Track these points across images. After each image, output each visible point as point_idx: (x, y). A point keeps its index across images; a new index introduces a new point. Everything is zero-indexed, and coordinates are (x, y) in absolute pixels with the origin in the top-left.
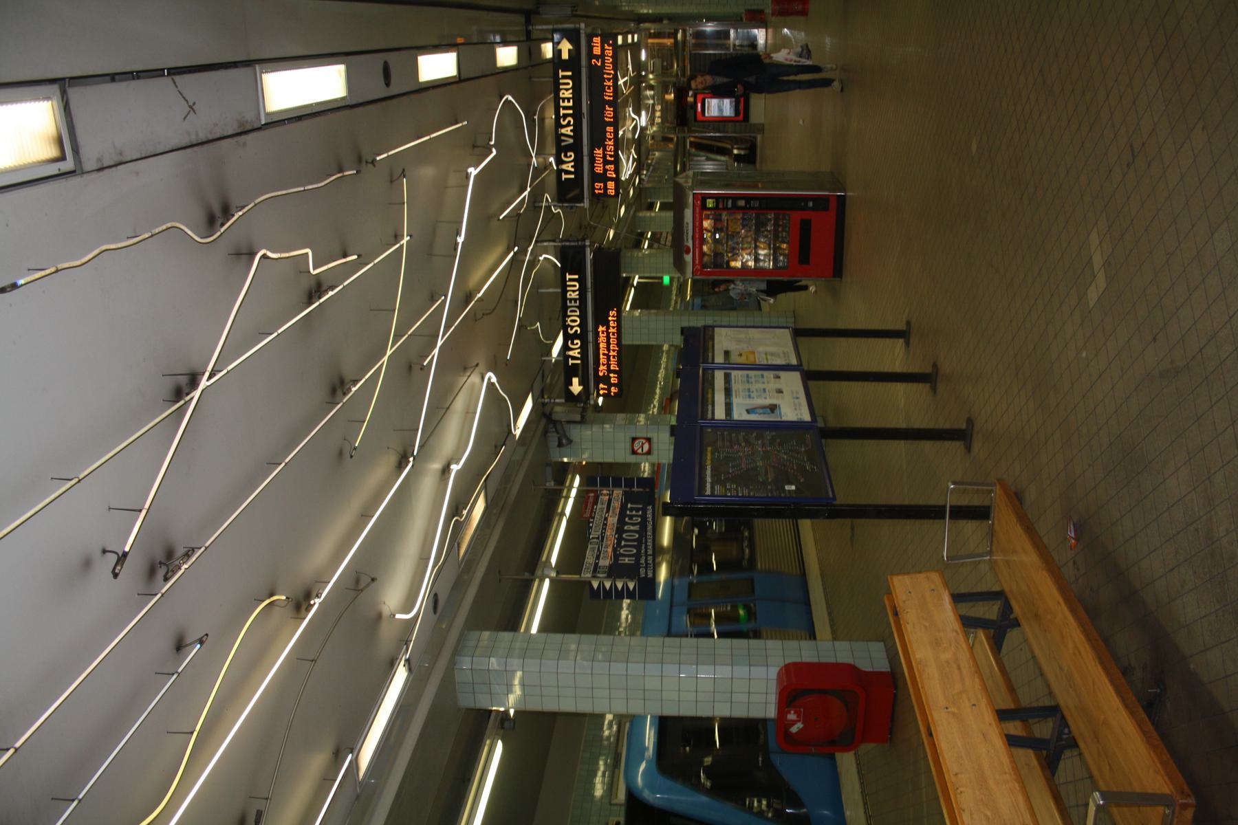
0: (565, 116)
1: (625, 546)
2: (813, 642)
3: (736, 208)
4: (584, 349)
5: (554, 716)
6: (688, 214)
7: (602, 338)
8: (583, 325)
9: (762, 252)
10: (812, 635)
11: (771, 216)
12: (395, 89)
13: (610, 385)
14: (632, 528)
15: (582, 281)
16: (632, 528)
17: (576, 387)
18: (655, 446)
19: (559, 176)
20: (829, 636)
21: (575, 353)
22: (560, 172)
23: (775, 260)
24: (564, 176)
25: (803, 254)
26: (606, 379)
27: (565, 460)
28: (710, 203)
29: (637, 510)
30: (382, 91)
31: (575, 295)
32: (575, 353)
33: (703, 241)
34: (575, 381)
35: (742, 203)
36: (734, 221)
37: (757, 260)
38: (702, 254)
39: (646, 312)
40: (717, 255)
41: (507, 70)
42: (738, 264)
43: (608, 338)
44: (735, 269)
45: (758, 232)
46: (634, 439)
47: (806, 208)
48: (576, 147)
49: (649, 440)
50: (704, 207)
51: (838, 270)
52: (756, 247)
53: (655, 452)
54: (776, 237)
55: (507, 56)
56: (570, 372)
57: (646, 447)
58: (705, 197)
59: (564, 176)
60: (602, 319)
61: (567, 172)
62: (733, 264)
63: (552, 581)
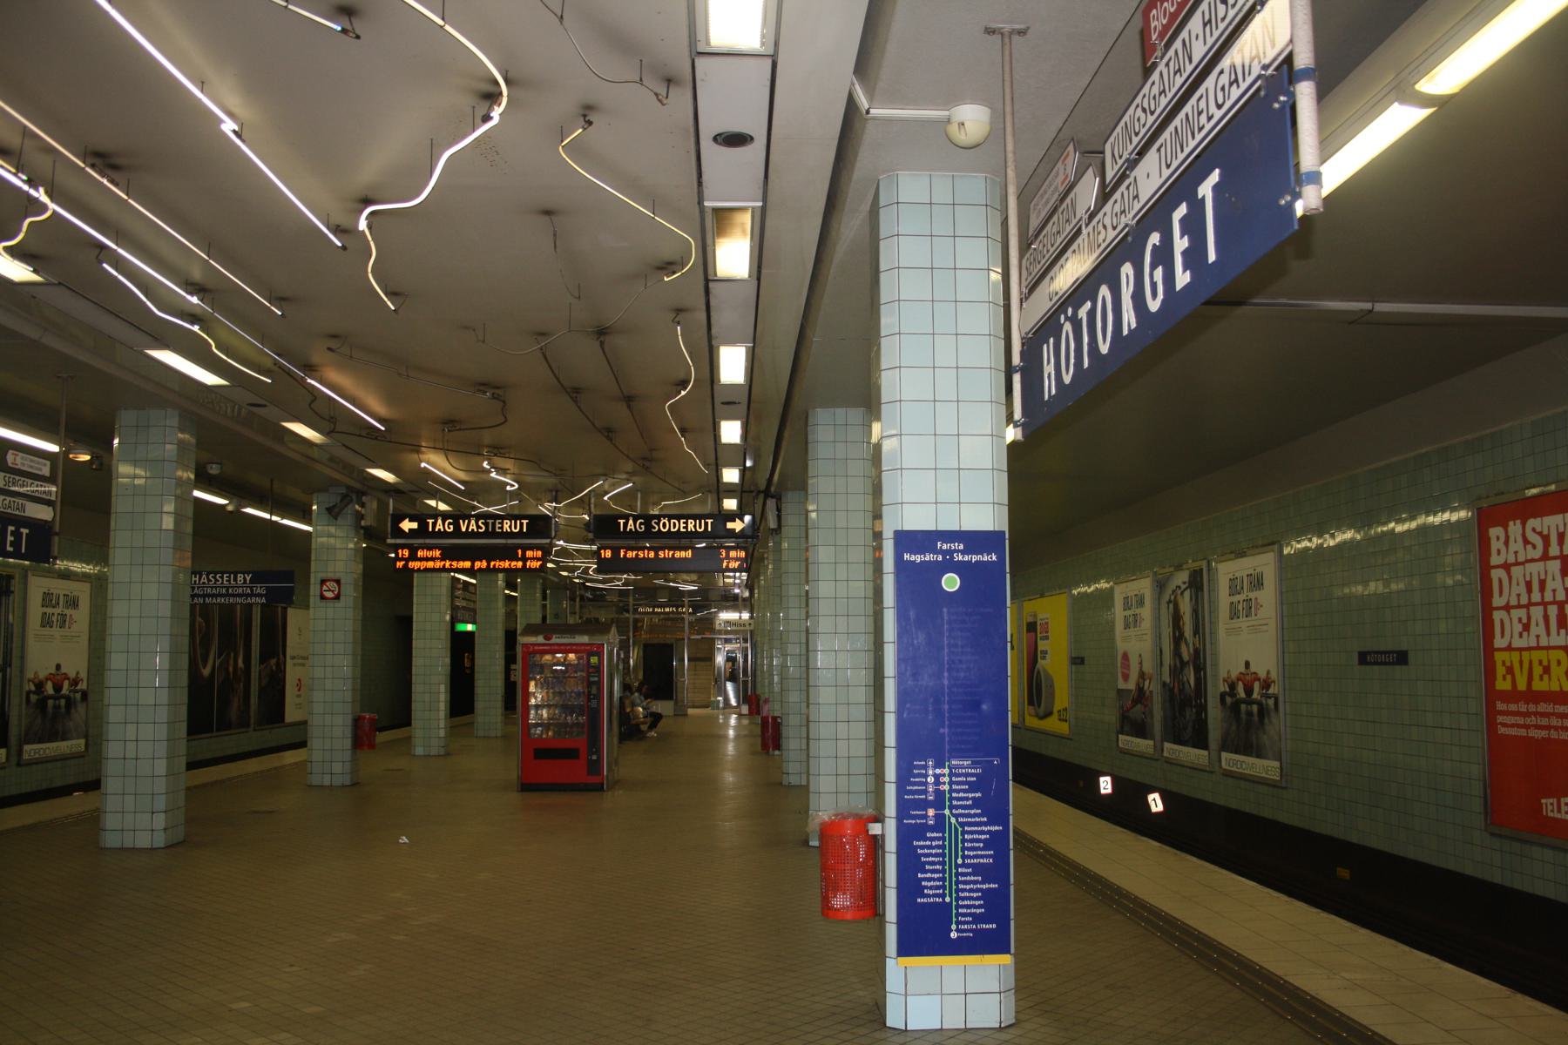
3: (590, 684)
5: (108, 513)
6: (585, 639)
9: (545, 713)
10: (191, 766)
11: (582, 719)
12: (710, 150)
13: (407, 560)
15: (520, 534)
17: (407, 525)
18: (330, 604)
20: (301, 751)
21: (439, 526)
22: (626, 517)
23: (537, 725)
25: (544, 753)
26: (413, 557)
27: (116, 441)
28: (594, 660)
30: (708, 128)
31: (506, 527)
32: (439, 526)
33: (554, 652)
34: (415, 525)
35: (594, 691)
36: (575, 686)
37: (537, 707)
39: (169, 541)
40: (542, 668)
41: (719, 476)
42: (532, 688)
44: (527, 687)
46: (338, 582)
48: (649, 534)
49: (337, 597)
50: (591, 654)
51: (526, 787)
52: (549, 706)
53: (323, 604)
54: (559, 725)
55: (731, 475)
56: (420, 518)
57: (329, 595)
58: (600, 655)
62: (532, 684)
63: (223, 506)
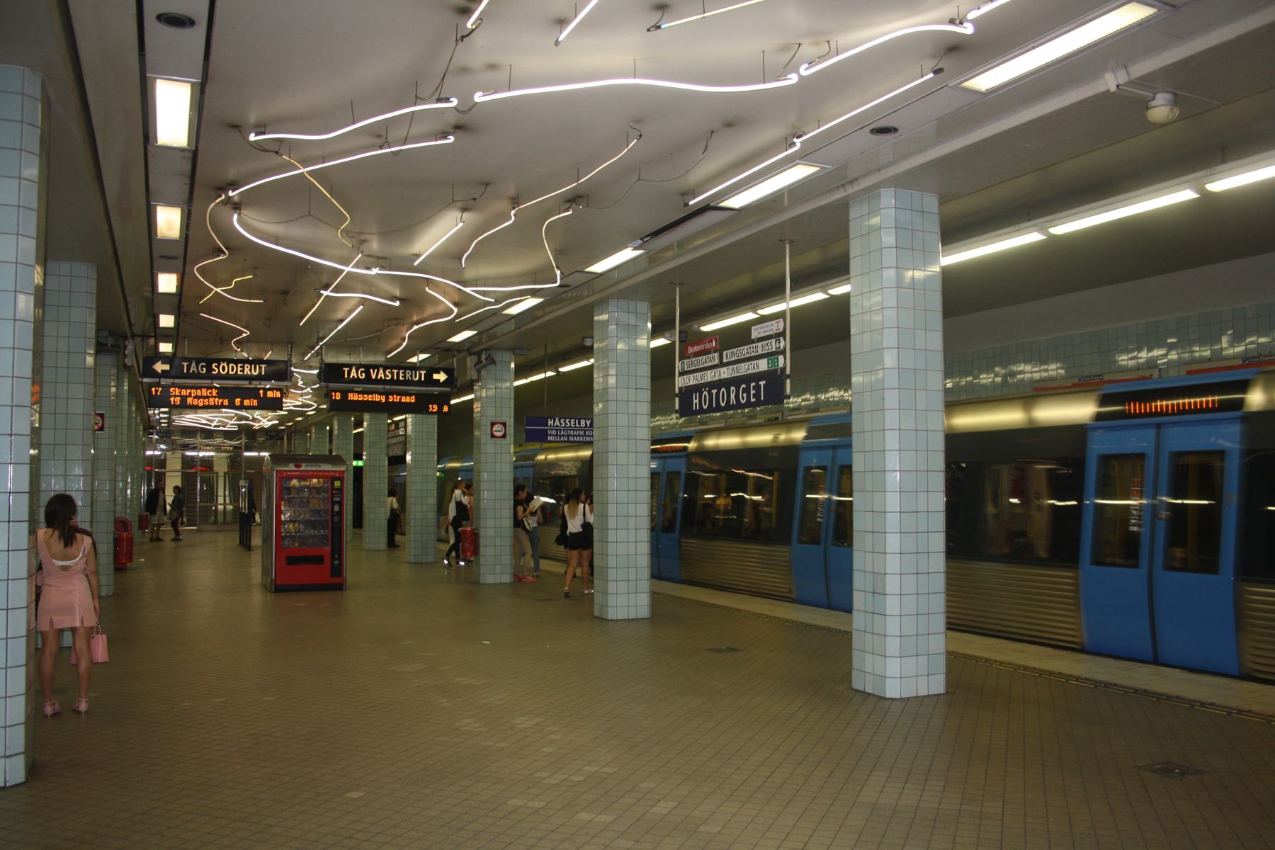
0: (392, 374)
1: (711, 395)
2: (941, 406)
3: (333, 503)
7: (205, 392)
8: (219, 377)
14: (732, 396)
16: (732, 396)
17: (442, 377)
19: (347, 365)
21: (354, 374)
24: (346, 369)
28: (337, 484)
29: (757, 395)
32: (354, 374)
38: (292, 478)
43: (205, 397)
45: (308, 523)
47: (333, 559)
53: (503, 420)
58: (341, 479)
59: (346, 369)
60: (222, 392)
61: (349, 373)
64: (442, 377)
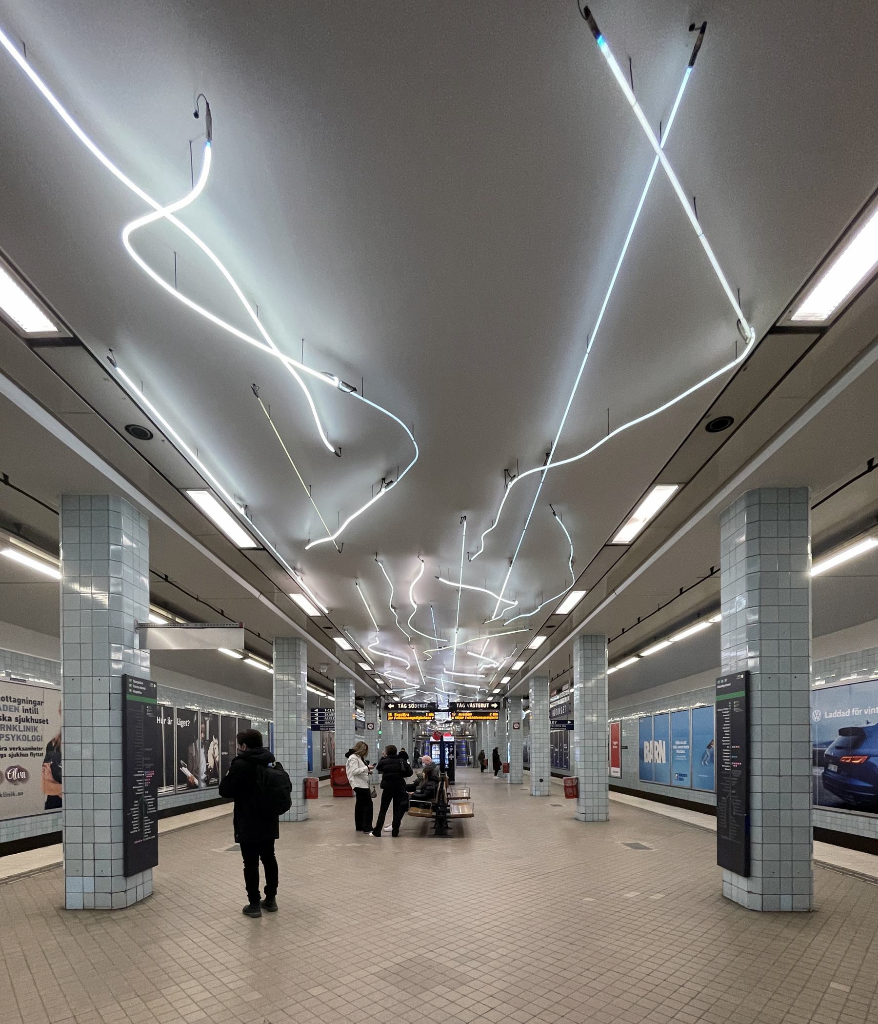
4: (404, 709)
17: (495, 705)
64: (495, 705)
